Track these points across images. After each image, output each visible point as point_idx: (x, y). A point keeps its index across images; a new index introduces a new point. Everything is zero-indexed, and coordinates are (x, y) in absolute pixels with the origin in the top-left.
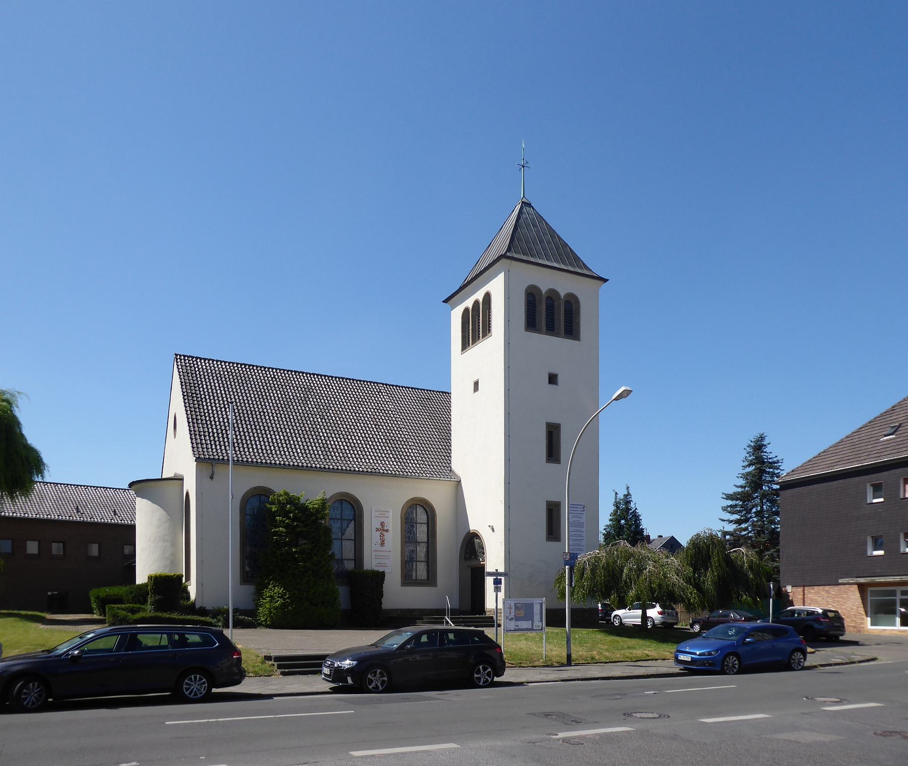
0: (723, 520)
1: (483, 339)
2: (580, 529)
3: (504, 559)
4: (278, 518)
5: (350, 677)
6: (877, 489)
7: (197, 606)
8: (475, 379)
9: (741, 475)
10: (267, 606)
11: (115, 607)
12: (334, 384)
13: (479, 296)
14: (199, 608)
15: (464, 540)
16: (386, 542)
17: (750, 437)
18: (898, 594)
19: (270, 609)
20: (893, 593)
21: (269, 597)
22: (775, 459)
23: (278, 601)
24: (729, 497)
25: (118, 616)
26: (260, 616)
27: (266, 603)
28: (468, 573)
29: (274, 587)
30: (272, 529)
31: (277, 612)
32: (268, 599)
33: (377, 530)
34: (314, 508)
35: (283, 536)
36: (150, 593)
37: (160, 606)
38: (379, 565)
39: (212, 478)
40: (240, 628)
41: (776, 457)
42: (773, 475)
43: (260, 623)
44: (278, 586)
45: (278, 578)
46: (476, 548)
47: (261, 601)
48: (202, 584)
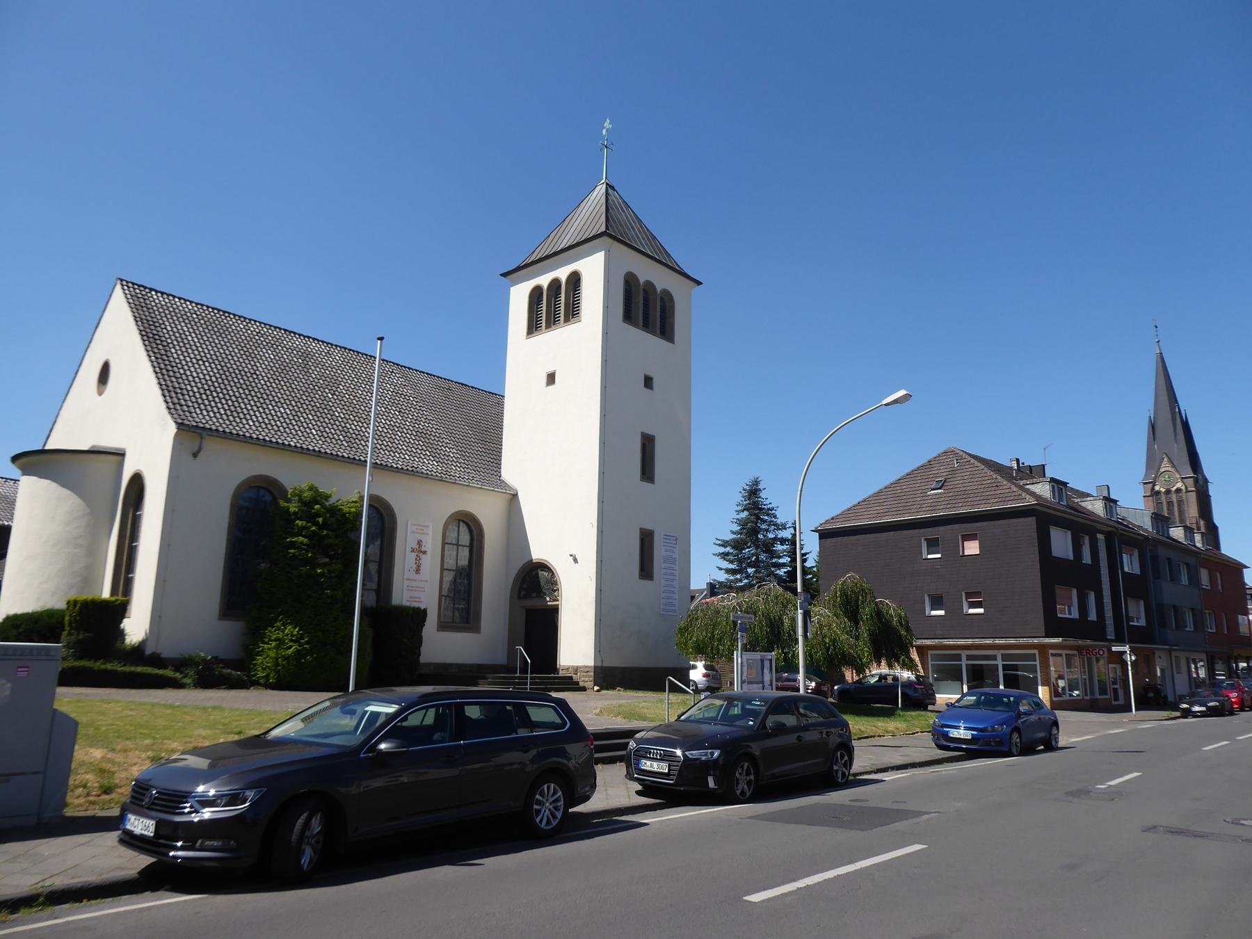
0: (721, 569)
2: (671, 566)
3: (594, 599)
4: (299, 523)
5: (712, 777)
6: (933, 545)
7: (148, 651)
8: (550, 370)
9: (735, 521)
10: (272, 654)
12: (336, 353)
13: (562, 273)
14: (150, 655)
15: (518, 575)
16: (422, 568)
17: (743, 482)
18: (964, 658)
19: (277, 659)
20: (959, 657)
22: (769, 506)
23: (291, 647)
24: (724, 544)
27: (269, 649)
28: (522, 617)
29: (284, 625)
30: (288, 538)
31: (288, 663)
32: (274, 644)
33: (413, 551)
34: (350, 513)
35: (304, 549)
36: (67, 628)
37: (82, 650)
38: (412, 599)
39: (195, 455)
40: (224, 689)
41: (770, 503)
42: (771, 523)
43: (254, 680)
44: (290, 624)
46: (542, 584)
48: (160, 617)
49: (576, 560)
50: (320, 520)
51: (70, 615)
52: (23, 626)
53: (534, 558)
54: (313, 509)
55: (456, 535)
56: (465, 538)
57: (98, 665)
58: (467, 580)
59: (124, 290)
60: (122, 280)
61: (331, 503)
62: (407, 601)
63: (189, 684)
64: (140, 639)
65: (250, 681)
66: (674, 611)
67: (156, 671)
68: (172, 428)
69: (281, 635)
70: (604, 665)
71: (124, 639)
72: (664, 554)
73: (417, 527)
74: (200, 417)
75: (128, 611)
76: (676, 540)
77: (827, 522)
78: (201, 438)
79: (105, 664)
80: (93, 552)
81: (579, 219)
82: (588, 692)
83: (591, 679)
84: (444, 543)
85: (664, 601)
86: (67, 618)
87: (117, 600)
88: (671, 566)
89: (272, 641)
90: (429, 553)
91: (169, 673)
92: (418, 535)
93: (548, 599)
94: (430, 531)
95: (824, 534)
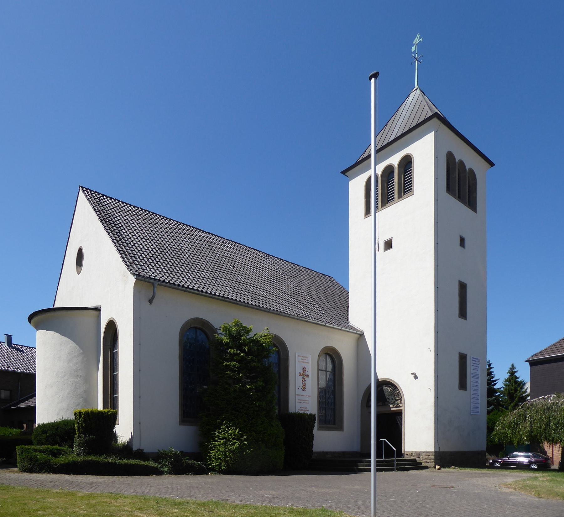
1: (399, 200)
2: (476, 380)
4: (232, 351)
7: (135, 448)
10: (222, 449)
11: (29, 449)
13: (395, 160)
16: (307, 387)
19: (225, 452)
21: (223, 438)
23: (234, 444)
25: (37, 460)
26: (211, 460)
27: (219, 445)
29: (227, 427)
30: (224, 363)
31: (234, 455)
36: (77, 432)
38: (301, 409)
39: (150, 301)
40: (192, 474)
44: (232, 426)
45: (231, 418)
47: (213, 444)
49: (416, 377)
50: (246, 348)
51: (78, 423)
52: (49, 432)
53: (379, 378)
54: (241, 340)
55: (325, 364)
56: (330, 367)
57: (102, 459)
58: (333, 395)
59: (85, 193)
60: (82, 188)
61: (251, 336)
62: (298, 410)
63: (166, 472)
64: (128, 440)
65: (207, 468)
66: (478, 412)
67: (143, 463)
68: (132, 280)
69: (226, 435)
70: (440, 451)
71: (117, 440)
72: (473, 371)
73: (302, 358)
74: (148, 273)
75: (117, 420)
76: (479, 361)
77: (536, 355)
78: (154, 287)
79: (106, 458)
80: (89, 380)
81: (401, 119)
82: (430, 469)
83: (433, 461)
84: (319, 370)
85: (472, 405)
86: (76, 425)
87: (109, 412)
88: (476, 380)
89: (220, 439)
90: (310, 376)
91: (151, 463)
92: (302, 363)
93: (391, 406)
94: (310, 360)
95: (533, 363)
